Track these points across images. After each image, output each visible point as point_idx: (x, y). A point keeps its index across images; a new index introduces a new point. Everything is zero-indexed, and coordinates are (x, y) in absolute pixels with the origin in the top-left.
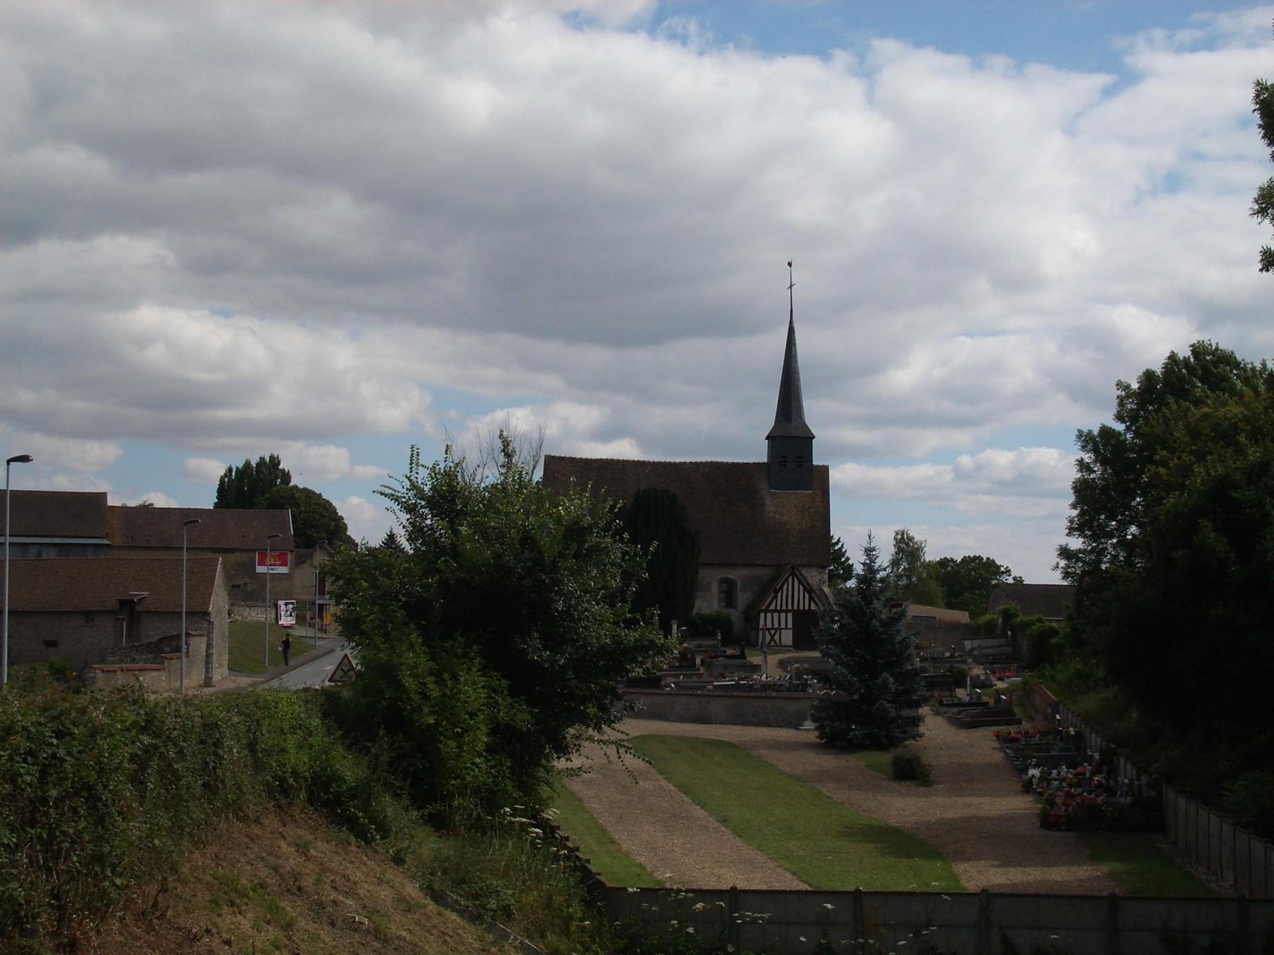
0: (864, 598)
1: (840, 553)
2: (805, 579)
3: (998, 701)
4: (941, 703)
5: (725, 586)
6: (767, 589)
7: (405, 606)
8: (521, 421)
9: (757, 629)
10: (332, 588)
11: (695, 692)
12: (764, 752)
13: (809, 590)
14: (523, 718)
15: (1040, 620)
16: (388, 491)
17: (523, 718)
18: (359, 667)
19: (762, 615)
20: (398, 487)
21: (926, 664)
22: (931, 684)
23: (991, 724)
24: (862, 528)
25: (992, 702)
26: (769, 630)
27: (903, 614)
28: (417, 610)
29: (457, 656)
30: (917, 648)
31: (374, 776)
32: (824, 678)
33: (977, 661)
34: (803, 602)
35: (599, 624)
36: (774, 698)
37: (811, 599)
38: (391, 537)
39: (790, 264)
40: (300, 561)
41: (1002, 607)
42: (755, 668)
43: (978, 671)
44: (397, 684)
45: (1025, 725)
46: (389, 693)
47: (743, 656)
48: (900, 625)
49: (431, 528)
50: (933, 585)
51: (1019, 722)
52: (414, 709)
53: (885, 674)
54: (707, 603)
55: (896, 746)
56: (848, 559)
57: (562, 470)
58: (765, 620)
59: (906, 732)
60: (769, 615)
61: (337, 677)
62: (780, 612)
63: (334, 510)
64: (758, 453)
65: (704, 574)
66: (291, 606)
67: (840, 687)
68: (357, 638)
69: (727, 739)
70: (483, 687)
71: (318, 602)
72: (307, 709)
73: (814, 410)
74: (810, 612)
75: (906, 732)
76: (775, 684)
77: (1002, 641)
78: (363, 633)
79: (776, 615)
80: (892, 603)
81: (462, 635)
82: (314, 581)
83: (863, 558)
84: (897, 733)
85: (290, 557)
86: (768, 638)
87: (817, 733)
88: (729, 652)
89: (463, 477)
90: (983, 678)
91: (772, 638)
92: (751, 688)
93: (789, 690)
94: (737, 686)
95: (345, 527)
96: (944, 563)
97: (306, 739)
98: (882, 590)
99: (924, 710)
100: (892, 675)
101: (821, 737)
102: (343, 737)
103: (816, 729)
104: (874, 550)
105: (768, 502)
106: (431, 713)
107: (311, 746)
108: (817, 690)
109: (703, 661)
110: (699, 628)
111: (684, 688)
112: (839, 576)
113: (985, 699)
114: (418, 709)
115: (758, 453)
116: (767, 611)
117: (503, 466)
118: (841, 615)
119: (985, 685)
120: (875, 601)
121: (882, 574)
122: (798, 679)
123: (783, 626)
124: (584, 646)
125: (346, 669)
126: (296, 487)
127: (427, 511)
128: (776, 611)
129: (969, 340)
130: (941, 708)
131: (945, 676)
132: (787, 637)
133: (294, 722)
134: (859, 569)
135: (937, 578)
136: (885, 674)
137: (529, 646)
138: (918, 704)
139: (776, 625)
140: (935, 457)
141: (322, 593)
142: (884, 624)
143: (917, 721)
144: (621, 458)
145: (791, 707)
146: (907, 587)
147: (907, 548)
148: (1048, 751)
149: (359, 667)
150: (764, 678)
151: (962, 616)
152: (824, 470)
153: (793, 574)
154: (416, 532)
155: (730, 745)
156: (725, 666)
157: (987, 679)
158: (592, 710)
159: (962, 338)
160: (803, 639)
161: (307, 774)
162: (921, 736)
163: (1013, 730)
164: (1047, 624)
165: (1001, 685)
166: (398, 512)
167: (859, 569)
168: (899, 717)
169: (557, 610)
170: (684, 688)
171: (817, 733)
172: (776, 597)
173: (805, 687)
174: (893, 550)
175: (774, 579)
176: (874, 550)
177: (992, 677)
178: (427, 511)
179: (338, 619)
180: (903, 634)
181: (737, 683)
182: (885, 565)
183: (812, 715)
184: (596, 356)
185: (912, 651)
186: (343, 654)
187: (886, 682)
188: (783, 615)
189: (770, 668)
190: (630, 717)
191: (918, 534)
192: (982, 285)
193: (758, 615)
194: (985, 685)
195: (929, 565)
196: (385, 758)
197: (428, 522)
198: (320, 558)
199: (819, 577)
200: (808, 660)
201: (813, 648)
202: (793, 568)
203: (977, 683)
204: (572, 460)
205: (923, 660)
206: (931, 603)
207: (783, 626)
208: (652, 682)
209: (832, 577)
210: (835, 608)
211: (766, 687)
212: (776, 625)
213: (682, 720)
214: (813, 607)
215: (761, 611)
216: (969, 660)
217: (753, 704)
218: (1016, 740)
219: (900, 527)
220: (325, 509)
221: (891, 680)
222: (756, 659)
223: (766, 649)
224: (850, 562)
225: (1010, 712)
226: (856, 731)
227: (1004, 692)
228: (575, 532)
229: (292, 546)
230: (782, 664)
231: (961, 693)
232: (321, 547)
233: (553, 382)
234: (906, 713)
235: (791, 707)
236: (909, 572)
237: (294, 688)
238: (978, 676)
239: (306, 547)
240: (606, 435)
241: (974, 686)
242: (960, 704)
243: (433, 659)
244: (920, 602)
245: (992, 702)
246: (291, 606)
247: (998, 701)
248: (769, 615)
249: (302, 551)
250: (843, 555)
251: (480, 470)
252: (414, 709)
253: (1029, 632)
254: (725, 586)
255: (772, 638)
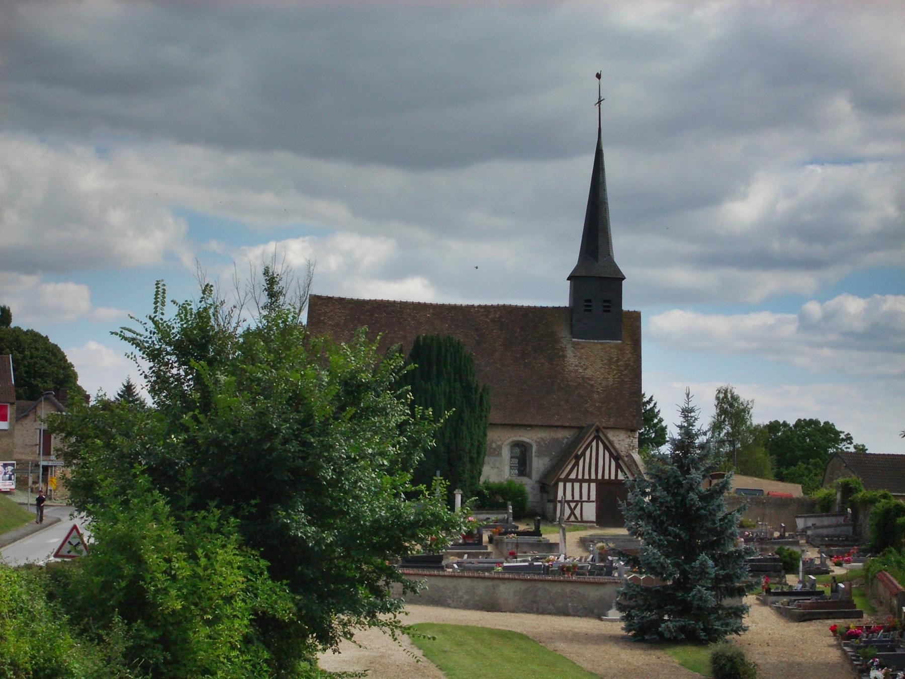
0: (680, 467)
1: (651, 415)
2: (611, 443)
3: (835, 590)
4: (768, 591)
5: (517, 451)
6: (567, 454)
7: (150, 470)
8: (294, 255)
9: (554, 501)
10: (60, 446)
11: (481, 574)
12: (561, 645)
13: (616, 457)
14: (285, 606)
15: (885, 496)
16: (129, 335)
17: (285, 606)
18: (92, 540)
19: (561, 485)
20: (140, 329)
21: (751, 546)
22: (758, 569)
23: (829, 616)
24: (678, 387)
25: (828, 591)
26: (568, 502)
27: (725, 486)
28: (163, 474)
29: (210, 530)
30: (742, 526)
31: (107, 670)
32: (633, 561)
33: (811, 542)
34: (608, 470)
35: (374, 490)
36: (575, 582)
37: (618, 466)
38: (129, 389)
39: (598, 76)
40: (21, 415)
41: (841, 480)
42: (552, 547)
43: (812, 554)
44: (138, 560)
45: (867, 619)
46: (128, 569)
47: (537, 533)
48: (722, 499)
49: (178, 378)
50: (761, 453)
51: (859, 615)
52: (157, 591)
53: (703, 556)
54: (497, 471)
55: (715, 640)
56: (661, 420)
57: (338, 315)
58: (564, 491)
59: (727, 625)
60: (569, 485)
61: (64, 551)
62: (581, 481)
63: (63, 358)
64: (559, 297)
65: (493, 436)
66: (10, 468)
67: (651, 569)
68: (89, 506)
69: (518, 630)
70: (239, 568)
71: (43, 463)
72: (29, 589)
73: (624, 246)
74: (617, 482)
75: (727, 625)
76: (575, 566)
77: (841, 520)
78: (96, 500)
79: (577, 485)
80: (712, 473)
81: (218, 507)
82: (37, 439)
83: (680, 420)
84: (717, 625)
85: (10, 411)
86: (567, 512)
87: (623, 624)
88: (522, 527)
89: (216, 320)
90: (817, 562)
91: (572, 513)
92: (546, 570)
93: (591, 573)
94: (531, 568)
95: (75, 376)
96: (774, 427)
97: (27, 625)
98: (702, 458)
99: (749, 599)
100: (713, 557)
101: (628, 629)
102: (71, 622)
103: (623, 619)
104: (692, 410)
105: (570, 353)
106: (178, 597)
107: (34, 634)
108: (623, 572)
109: (491, 540)
110: (488, 499)
111: (469, 569)
112: (652, 441)
113: (819, 587)
114: (165, 591)
115: (559, 297)
116: (566, 480)
117: (265, 307)
118: (654, 487)
119: (821, 571)
120: (693, 471)
121: (702, 439)
122: (602, 560)
123: (585, 498)
124: (356, 519)
125: (74, 542)
126: (18, 329)
127: (174, 358)
128: (576, 480)
129: (818, 169)
130: (768, 596)
131: (775, 560)
132: (590, 511)
133: (14, 604)
134: (673, 432)
135: (765, 445)
136: (703, 556)
137: (292, 520)
138: (741, 592)
139: (577, 498)
140: (774, 303)
141: (47, 452)
142: (703, 498)
143: (739, 612)
144: (398, 299)
145: (593, 593)
146: (730, 455)
147: (731, 409)
148: (892, 649)
149: (92, 540)
150: (562, 559)
151: (794, 490)
152: (635, 317)
153: (597, 438)
154: (160, 383)
155: (523, 637)
156: (517, 545)
157: (823, 563)
158: (362, 592)
159: (811, 167)
160: (608, 514)
161: (29, 666)
162: (745, 630)
163: (852, 624)
164: (894, 501)
165: (838, 571)
166: (139, 360)
167: (673, 432)
168: (720, 607)
169: (325, 479)
170: (469, 569)
171: (623, 624)
172: (577, 464)
173: (610, 570)
174: (714, 411)
175: (577, 441)
176: (692, 410)
177: (828, 562)
178: (174, 358)
179: (68, 483)
180: (726, 509)
181: (531, 565)
182: (705, 428)
183: (618, 603)
184: (388, 180)
185: (735, 529)
186: (70, 525)
187: (703, 564)
188: (585, 485)
189: (569, 546)
190: (411, 602)
191: (744, 393)
192: (841, 105)
193: (556, 485)
194: (821, 571)
195: (756, 431)
196: (120, 647)
197: (174, 371)
198: (45, 410)
199: (628, 441)
200: (614, 538)
201: (619, 524)
202: (598, 430)
203: (811, 569)
204: (341, 300)
205: (748, 540)
206: (759, 474)
207: (585, 498)
208: (432, 562)
209: (643, 442)
210: (646, 477)
211: (564, 569)
212: (577, 498)
213: (466, 606)
214: (621, 477)
215: (559, 480)
216: (802, 542)
217: (550, 589)
218: (856, 636)
219: (723, 385)
220: (54, 355)
221: (710, 563)
222: (551, 535)
223: (564, 525)
224: (664, 424)
225: (849, 603)
226: (669, 624)
227: (842, 579)
228: (352, 390)
229: (13, 400)
230: (584, 543)
231: (792, 580)
232: (47, 399)
233: (339, 211)
234: (728, 602)
235: (593, 593)
236: (732, 437)
237: (13, 565)
238: (812, 560)
239: (28, 399)
240: (395, 272)
241: (807, 572)
242: (791, 593)
243: (181, 532)
244: (745, 472)
245: (828, 591)
246: (10, 468)
247: (835, 590)
248: (569, 485)
249: (24, 403)
250: (656, 416)
251: (236, 311)
252: (157, 591)
253: (873, 509)
254: (517, 451)
255: (572, 513)
